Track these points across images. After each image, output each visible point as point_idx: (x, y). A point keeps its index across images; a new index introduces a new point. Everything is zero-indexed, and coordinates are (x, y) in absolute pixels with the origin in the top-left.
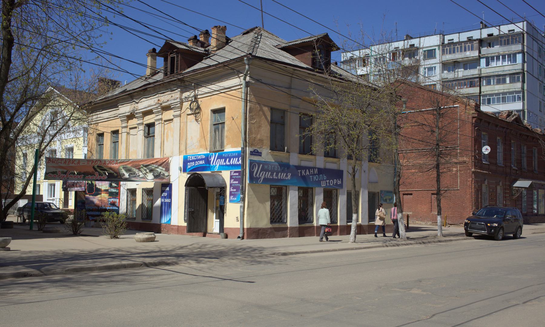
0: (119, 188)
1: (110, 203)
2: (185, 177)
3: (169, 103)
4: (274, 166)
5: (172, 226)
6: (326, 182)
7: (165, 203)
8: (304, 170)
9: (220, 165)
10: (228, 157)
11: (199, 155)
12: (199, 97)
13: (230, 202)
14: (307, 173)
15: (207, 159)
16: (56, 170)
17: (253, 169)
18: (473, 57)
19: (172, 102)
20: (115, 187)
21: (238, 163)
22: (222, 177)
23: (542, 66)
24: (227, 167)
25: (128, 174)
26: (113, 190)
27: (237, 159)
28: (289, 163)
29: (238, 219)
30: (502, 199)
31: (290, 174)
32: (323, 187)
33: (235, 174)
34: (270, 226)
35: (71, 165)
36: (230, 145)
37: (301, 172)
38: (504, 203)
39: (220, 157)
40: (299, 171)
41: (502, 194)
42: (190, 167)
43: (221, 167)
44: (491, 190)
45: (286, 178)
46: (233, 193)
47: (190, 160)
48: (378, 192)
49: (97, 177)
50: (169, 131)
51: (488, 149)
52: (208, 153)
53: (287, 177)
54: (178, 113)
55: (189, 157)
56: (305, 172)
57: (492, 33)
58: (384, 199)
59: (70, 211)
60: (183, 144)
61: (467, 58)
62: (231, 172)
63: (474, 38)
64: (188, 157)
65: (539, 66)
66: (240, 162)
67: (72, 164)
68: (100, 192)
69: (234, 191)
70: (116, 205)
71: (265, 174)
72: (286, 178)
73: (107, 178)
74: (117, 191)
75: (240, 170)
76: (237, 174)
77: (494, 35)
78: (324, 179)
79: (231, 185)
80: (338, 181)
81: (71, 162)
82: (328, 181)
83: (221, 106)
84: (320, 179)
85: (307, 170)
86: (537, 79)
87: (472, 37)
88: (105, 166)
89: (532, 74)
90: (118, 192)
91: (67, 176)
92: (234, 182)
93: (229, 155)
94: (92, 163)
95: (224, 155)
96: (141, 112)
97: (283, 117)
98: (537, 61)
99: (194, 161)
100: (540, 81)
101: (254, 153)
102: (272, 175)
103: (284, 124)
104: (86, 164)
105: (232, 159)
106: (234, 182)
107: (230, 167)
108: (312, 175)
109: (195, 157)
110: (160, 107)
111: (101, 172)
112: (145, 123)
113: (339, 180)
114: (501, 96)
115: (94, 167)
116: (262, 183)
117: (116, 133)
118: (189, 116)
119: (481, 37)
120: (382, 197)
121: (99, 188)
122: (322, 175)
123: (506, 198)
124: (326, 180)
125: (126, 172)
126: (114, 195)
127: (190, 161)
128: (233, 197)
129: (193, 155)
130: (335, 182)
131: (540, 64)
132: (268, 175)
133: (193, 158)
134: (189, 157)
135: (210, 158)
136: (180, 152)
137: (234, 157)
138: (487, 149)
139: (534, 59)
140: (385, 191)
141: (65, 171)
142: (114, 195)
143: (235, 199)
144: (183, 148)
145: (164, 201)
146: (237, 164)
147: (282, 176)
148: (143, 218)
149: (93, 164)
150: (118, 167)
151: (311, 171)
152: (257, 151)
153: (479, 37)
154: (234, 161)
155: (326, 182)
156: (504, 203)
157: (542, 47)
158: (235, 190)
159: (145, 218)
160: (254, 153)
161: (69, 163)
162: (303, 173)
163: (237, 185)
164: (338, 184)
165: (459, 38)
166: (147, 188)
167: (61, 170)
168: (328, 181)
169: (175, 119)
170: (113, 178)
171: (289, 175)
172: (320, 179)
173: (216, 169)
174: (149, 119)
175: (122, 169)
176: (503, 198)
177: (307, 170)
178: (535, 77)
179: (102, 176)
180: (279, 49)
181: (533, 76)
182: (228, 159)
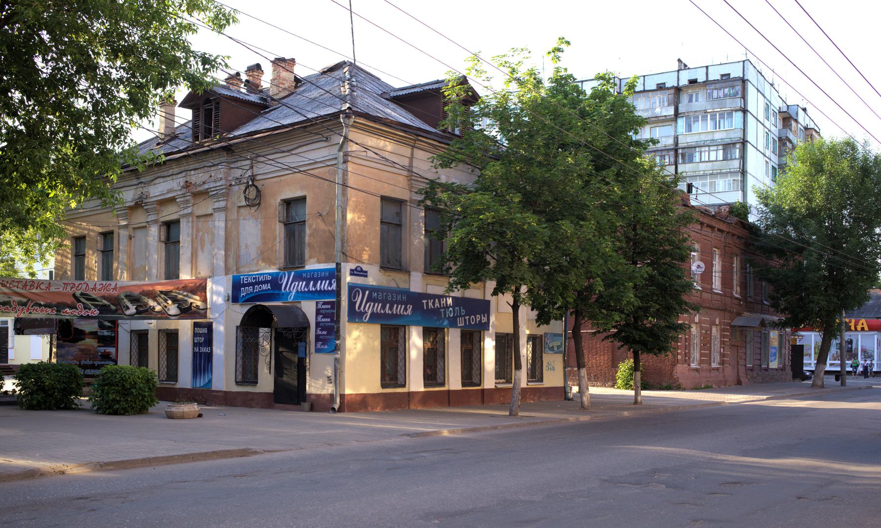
0: (116, 329)
1: (100, 354)
2: (240, 311)
3: (206, 186)
4: (387, 294)
5: (214, 391)
6: (465, 320)
7: (201, 354)
8: (432, 300)
9: (297, 291)
10: (312, 278)
11: (261, 274)
12: (258, 177)
13: (316, 352)
14: (436, 305)
15: (275, 282)
16: (8, 299)
17: (354, 298)
18: (665, 116)
19: (211, 186)
20: (108, 328)
21: (329, 288)
22: (302, 311)
23: (769, 133)
24: (310, 295)
25: (135, 307)
26: (106, 333)
27: (328, 281)
28: (409, 289)
29: (331, 380)
30: (719, 345)
31: (411, 306)
32: (460, 327)
33: (324, 307)
34: (379, 390)
35: (34, 291)
36: (315, 259)
37: (427, 303)
38: (722, 351)
39: (298, 278)
40: (424, 301)
41: (719, 336)
42: (244, 294)
43: (300, 295)
44: (704, 332)
45: (405, 313)
46: (322, 337)
47: (245, 282)
48: (542, 335)
49: (81, 312)
50: (206, 235)
51: (701, 266)
52: (277, 271)
53: (406, 312)
54: (222, 204)
55: (243, 278)
56: (434, 304)
57: (695, 78)
58: (551, 346)
59: (11, 369)
60: (232, 255)
61: (656, 117)
62: (317, 303)
63: (667, 85)
64: (242, 277)
65: (765, 134)
66: (334, 286)
67: (37, 289)
68: (82, 337)
69: (323, 335)
70: (111, 358)
71: (374, 306)
72: (405, 313)
73: (99, 314)
74: (113, 335)
75: (335, 300)
76: (329, 306)
77: (698, 81)
78: (462, 314)
79: (318, 324)
80: (483, 318)
81: (36, 285)
82: (468, 317)
83: (299, 194)
84: (455, 315)
85: (437, 300)
86: (763, 154)
87: (664, 83)
88: (94, 294)
89: (756, 146)
90: (114, 336)
91: (28, 309)
92: (323, 320)
93: (313, 275)
94: (72, 288)
95: (304, 275)
96: (155, 201)
97: (399, 214)
98: (763, 125)
99: (252, 284)
100: (768, 158)
101: (355, 272)
102: (383, 307)
103: (399, 226)
104: (61, 289)
105: (319, 282)
106: (323, 320)
107: (317, 295)
108: (443, 308)
109: (254, 278)
110: (189, 194)
111: (88, 303)
112: (162, 220)
113: (484, 316)
114: (708, 181)
115: (74, 295)
116: (368, 322)
117: (107, 236)
118: (242, 210)
119: (678, 83)
120: (547, 343)
121: (81, 330)
122: (458, 308)
123: (724, 344)
124: (464, 316)
125: (131, 303)
126: (108, 340)
127: (245, 285)
128: (322, 344)
129: (250, 275)
130: (478, 320)
131: (767, 131)
132: (378, 308)
133: (249, 279)
134: (243, 278)
135: (281, 280)
136: (227, 271)
137: (322, 279)
138: (699, 267)
139: (758, 122)
140: (551, 334)
141: (25, 300)
142: (108, 340)
143: (326, 347)
144: (231, 262)
145: (199, 350)
146: (328, 291)
147: (399, 309)
148: (238, 380)
149: (74, 289)
150: (116, 295)
151: (442, 302)
152: (361, 268)
153: (676, 85)
154: (323, 285)
155: (465, 320)
156: (722, 351)
157: (771, 104)
158: (325, 333)
159: (164, 379)
160: (355, 272)
161: (32, 287)
162: (430, 304)
163: (329, 324)
164: (483, 322)
165: (644, 84)
166: (167, 330)
167: (17, 299)
168: (467, 318)
169: (216, 214)
170: (106, 314)
171: (409, 307)
172: (455, 315)
173: (291, 298)
174: (169, 213)
175: (124, 298)
176: (721, 344)
177: (437, 300)
178: (760, 151)
179: (90, 309)
180: (386, 99)
181: (756, 148)
182: (312, 282)
